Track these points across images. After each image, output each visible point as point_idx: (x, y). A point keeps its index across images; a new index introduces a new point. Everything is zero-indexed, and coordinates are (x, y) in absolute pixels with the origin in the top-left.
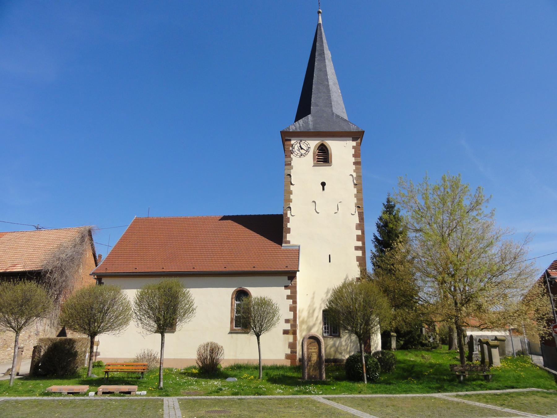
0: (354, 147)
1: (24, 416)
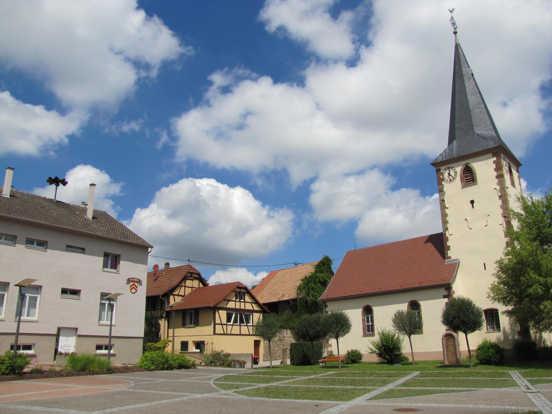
0: (494, 162)
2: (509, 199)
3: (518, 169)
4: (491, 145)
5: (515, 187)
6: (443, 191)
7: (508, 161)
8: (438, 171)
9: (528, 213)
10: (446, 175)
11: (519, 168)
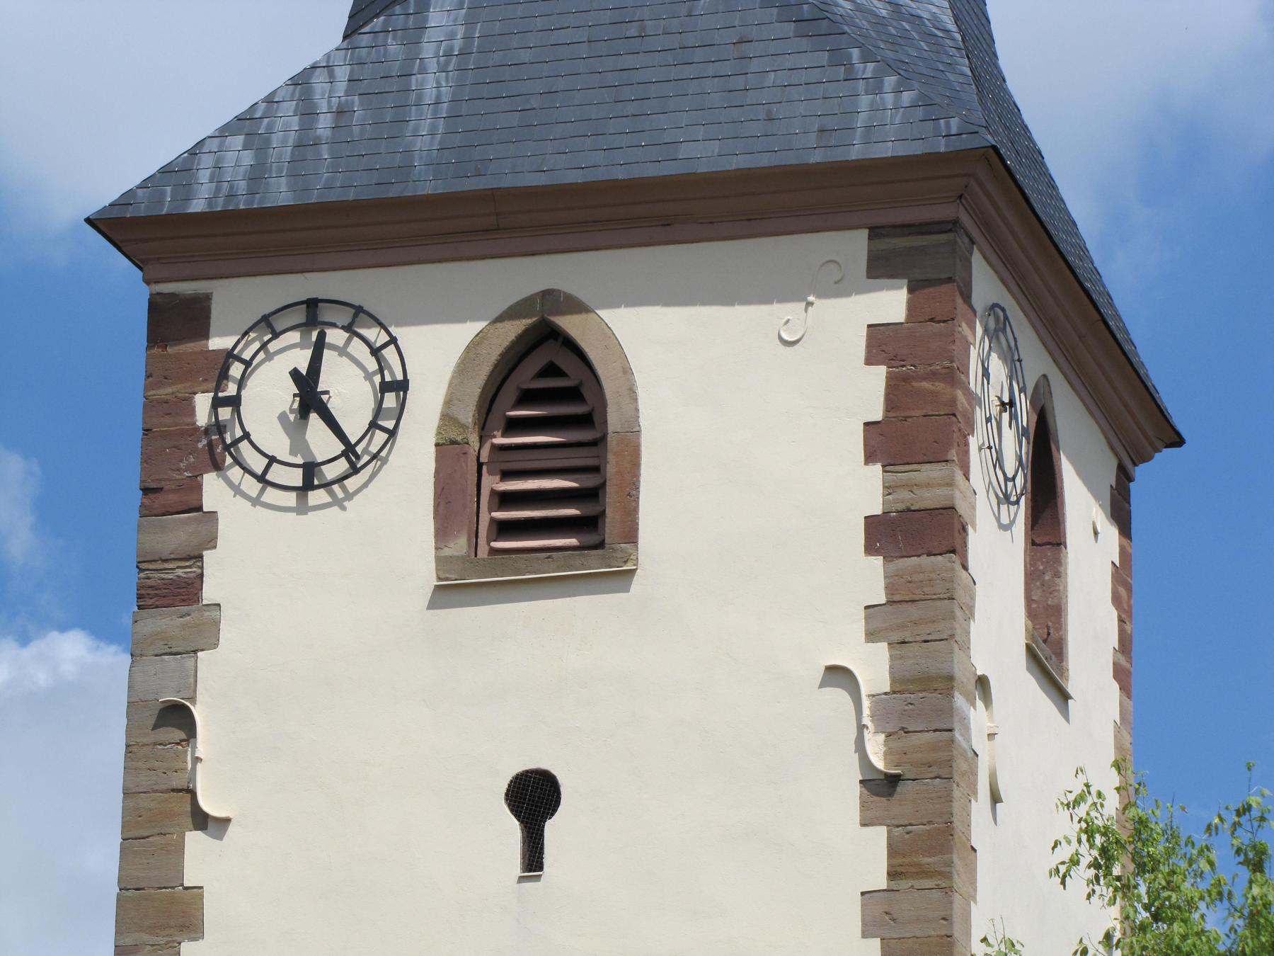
0: (881, 343)
1: (684, 8)
2: (980, 825)
3: (1124, 476)
4: (882, 121)
5: (1062, 696)
6: (186, 591)
7: (1037, 361)
8: (175, 322)
9: (1051, 197)
10: (267, 393)
11: (1141, 472)
